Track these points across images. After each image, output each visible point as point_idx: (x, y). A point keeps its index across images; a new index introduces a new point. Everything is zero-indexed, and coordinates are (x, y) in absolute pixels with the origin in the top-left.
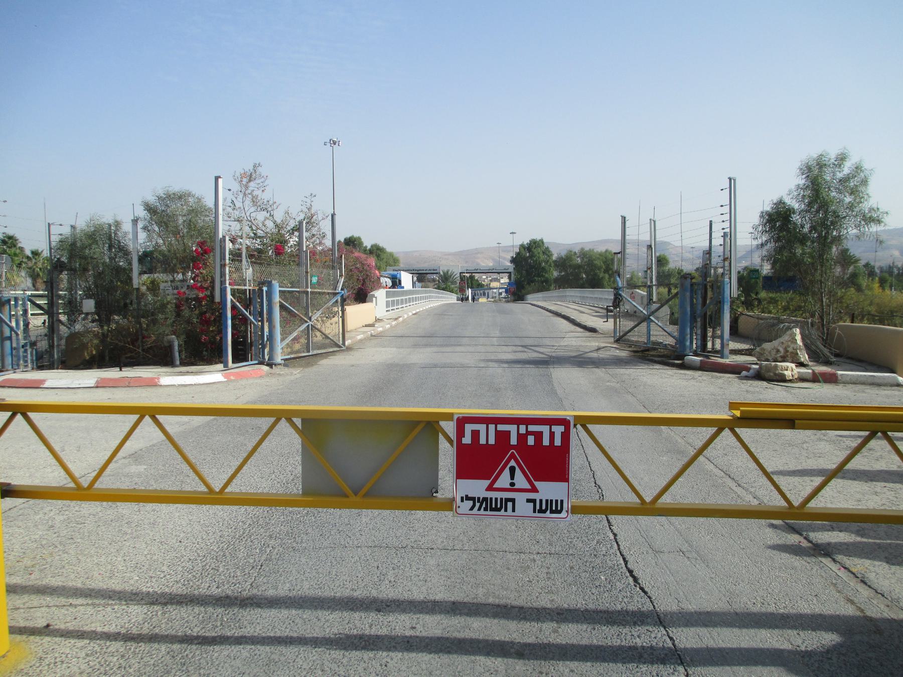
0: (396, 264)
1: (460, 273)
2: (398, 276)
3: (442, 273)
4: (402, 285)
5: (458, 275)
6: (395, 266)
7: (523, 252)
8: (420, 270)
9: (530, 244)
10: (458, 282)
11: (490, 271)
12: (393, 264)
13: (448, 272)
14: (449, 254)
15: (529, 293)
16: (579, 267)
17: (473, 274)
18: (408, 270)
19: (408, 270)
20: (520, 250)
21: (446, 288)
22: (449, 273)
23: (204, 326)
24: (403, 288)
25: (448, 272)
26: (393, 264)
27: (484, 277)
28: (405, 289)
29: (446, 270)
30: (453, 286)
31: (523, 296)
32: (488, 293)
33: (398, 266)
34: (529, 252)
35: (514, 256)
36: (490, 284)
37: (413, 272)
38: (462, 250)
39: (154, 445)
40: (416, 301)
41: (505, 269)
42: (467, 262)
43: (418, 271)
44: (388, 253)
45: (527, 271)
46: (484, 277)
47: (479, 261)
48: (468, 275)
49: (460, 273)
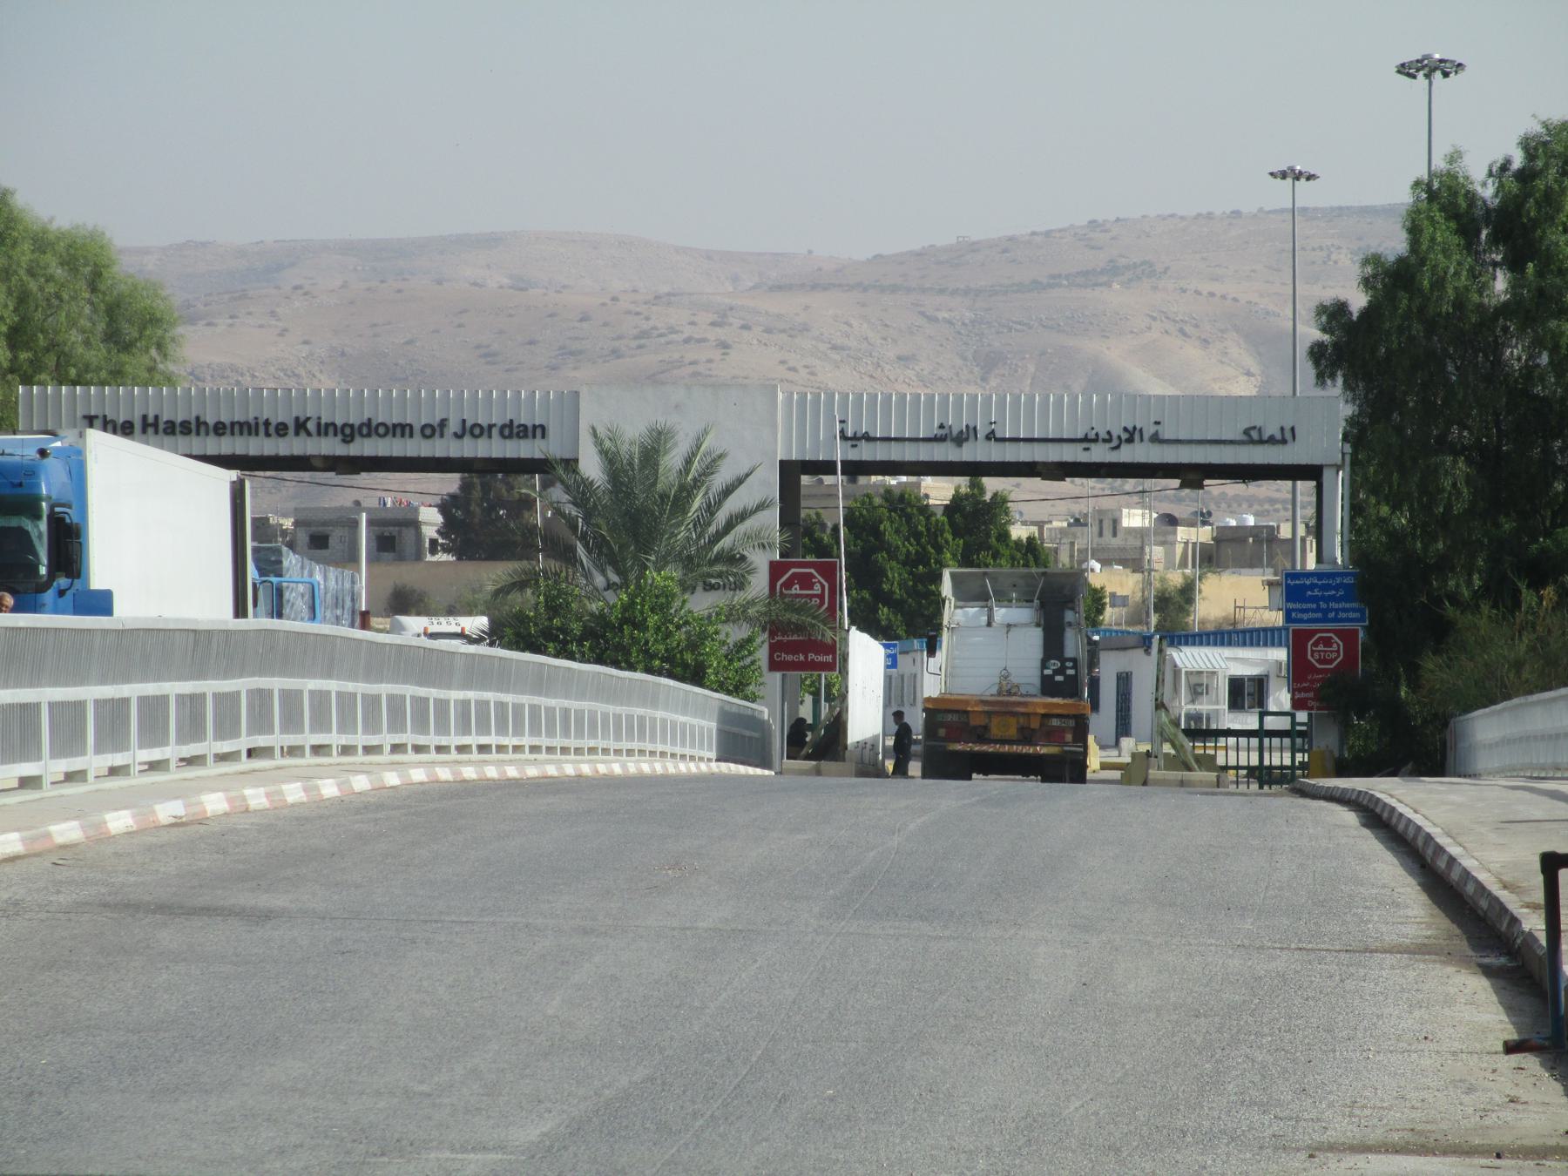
0: (135, 363)
1: (791, 472)
2: (51, 484)
3: (592, 467)
4: (99, 575)
5: (767, 484)
6: (117, 375)
7: (1452, 263)
8: (369, 429)
9: (1525, 176)
10: (760, 561)
11: (1099, 454)
12: (96, 355)
13: (651, 453)
14: (819, 282)
15: (1491, 693)
16: (1523, 932)
17: (992, 485)
18: (186, 428)
19: (171, 429)
20: (1414, 231)
21: (629, 618)
22: (672, 461)
23: (1105, 604)
24: (101, 603)
25: (651, 453)
26: (96, 355)
27: (1134, 518)
28: (129, 610)
29: (632, 430)
30: (701, 603)
31: (1442, 722)
32: (1124, 681)
33: (152, 375)
34: (1515, 264)
35: (1358, 301)
36: (1187, 593)
37: (227, 445)
38: (944, 237)
39: (922, 918)
40: (484, 728)
41: (1252, 437)
42: (989, 363)
43: (348, 433)
44: (42, 242)
45: (1486, 460)
46: (1134, 518)
47: (1114, 353)
48: (938, 491)
49: (791, 472)
